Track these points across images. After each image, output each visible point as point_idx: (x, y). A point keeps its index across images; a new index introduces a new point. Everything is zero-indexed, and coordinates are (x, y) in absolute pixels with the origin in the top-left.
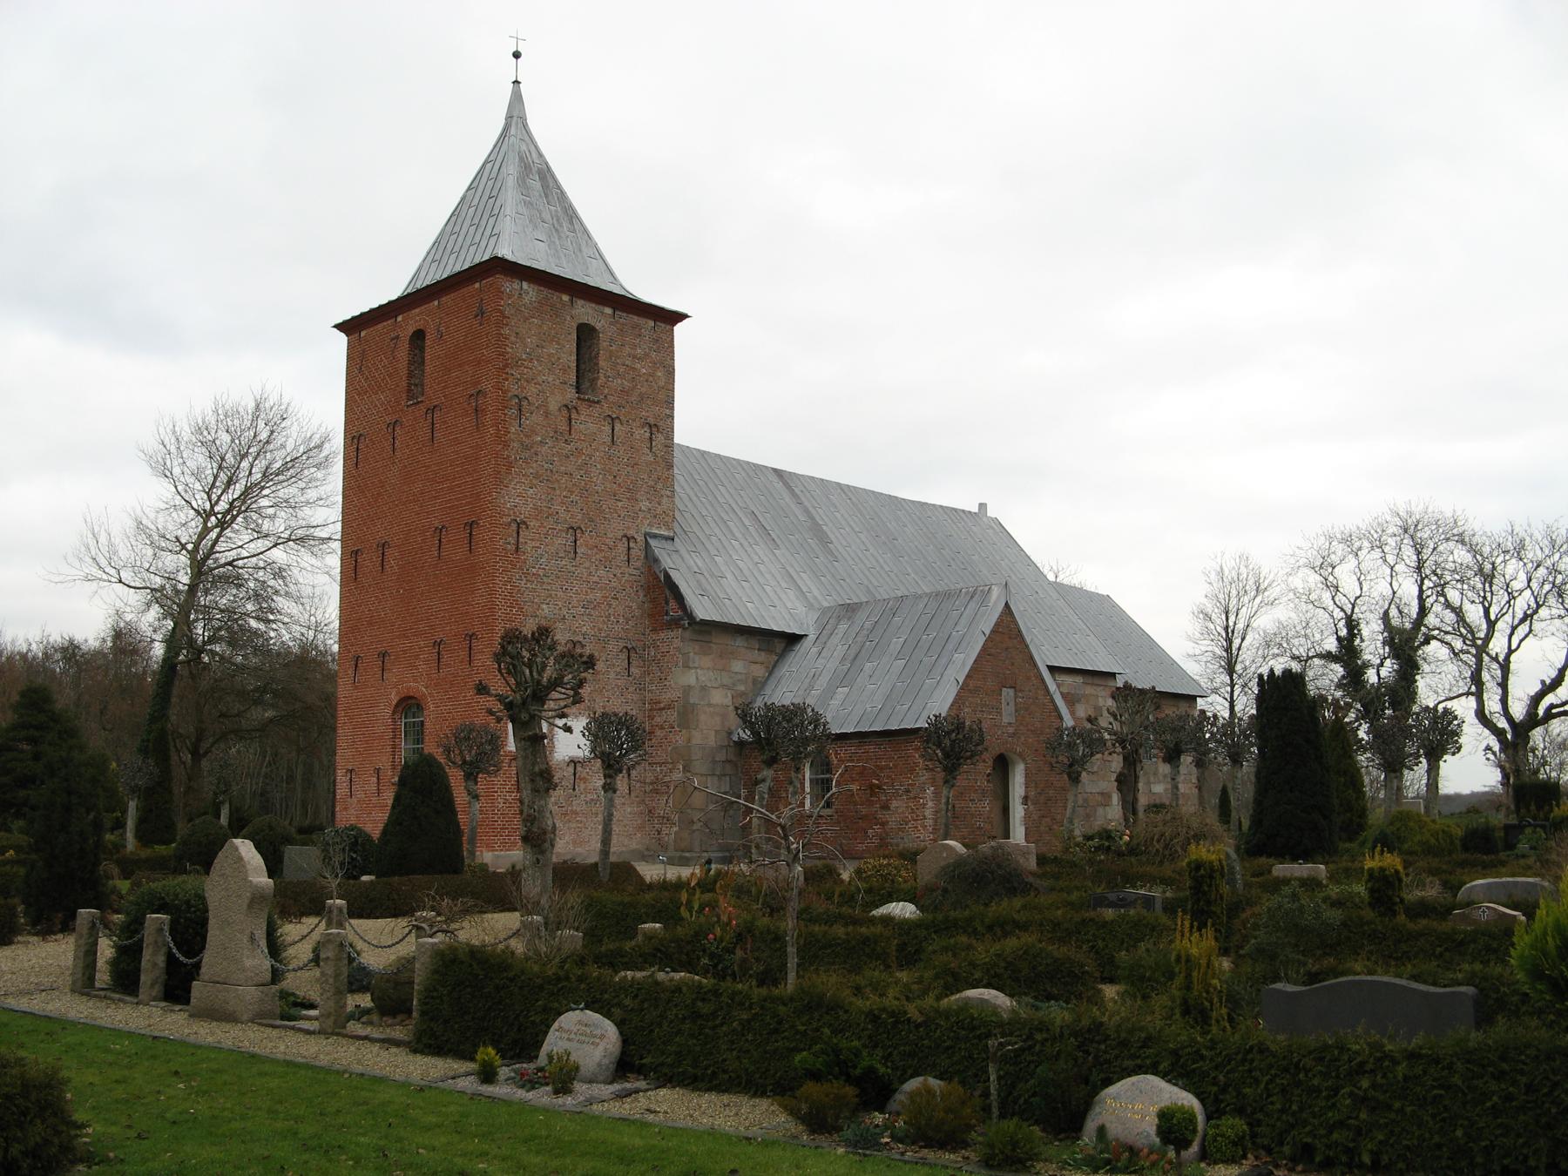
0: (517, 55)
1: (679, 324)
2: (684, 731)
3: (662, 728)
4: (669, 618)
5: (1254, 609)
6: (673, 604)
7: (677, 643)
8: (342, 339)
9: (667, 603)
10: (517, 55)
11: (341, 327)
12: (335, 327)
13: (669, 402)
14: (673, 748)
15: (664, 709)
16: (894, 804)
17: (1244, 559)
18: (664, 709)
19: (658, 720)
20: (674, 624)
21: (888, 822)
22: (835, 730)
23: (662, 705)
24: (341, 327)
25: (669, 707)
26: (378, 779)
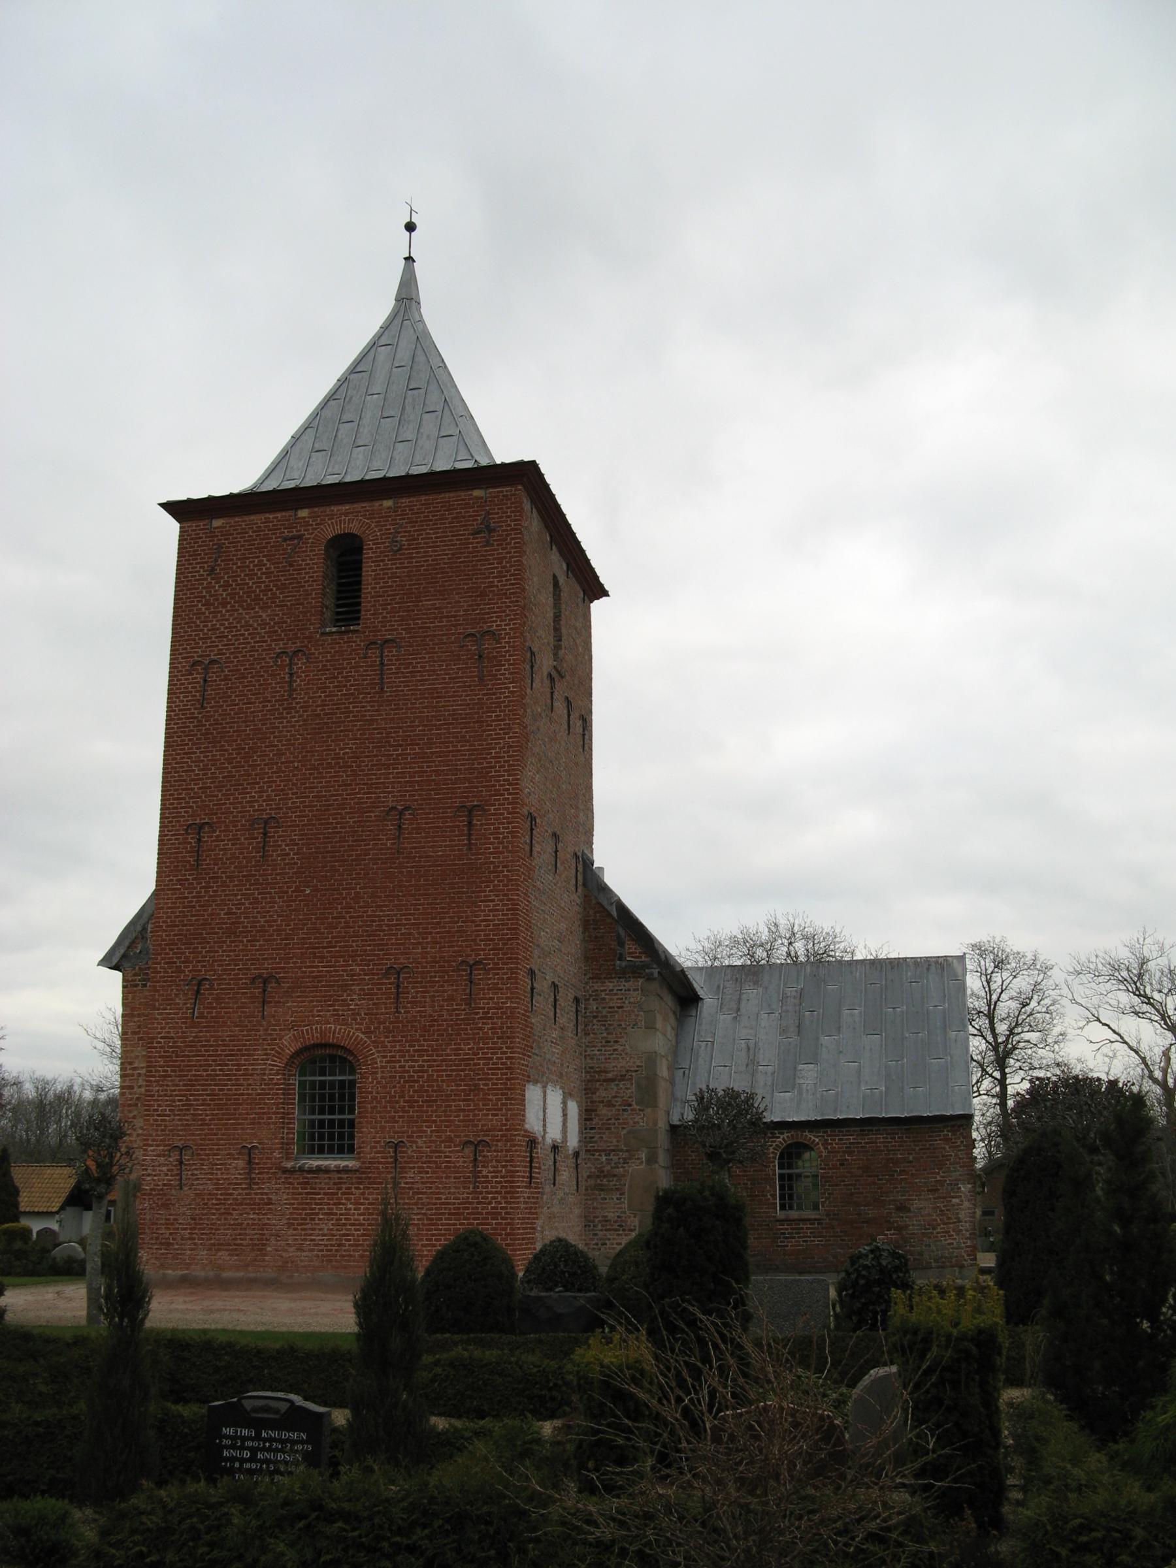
0: (410, 227)
1: (596, 602)
2: (649, 1110)
3: (609, 1104)
4: (624, 964)
5: (1153, 1011)
6: (630, 946)
7: (635, 996)
8: (172, 527)
9: (621, 944)
10: (410, 227)
11: (172, 508)
12: (162, 505)
13: (177, 599)
14: (629, 1132)
15: (613, 1080)
16: (916, 1204)
17: (1003, 940)
18: (613, 1080)
19: (602, 1093)
20: (635, 971)
21: (906, 1227)
22: (769, 1117)
23: (610, 1075)
24: (172, 508)
25: (622, 1078)
26: (250, 1162)
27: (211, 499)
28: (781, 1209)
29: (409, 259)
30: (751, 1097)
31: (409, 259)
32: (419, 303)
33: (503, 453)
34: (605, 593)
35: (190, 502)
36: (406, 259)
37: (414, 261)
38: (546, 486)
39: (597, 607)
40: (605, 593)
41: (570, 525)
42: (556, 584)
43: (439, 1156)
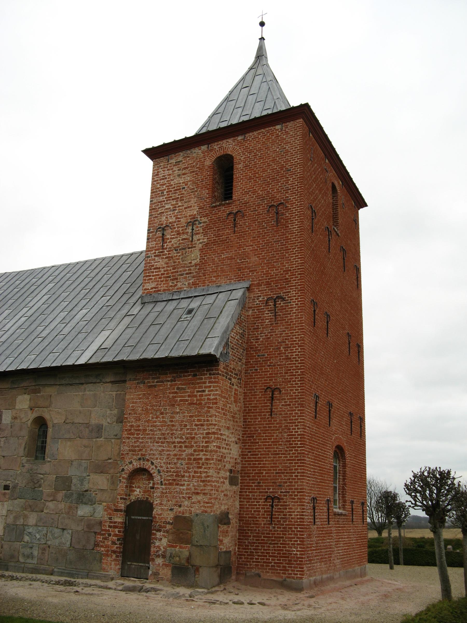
0: (262, 24)
8: (148, 163)
10: (262, 24)
27: (165, 145)
28: (336, 487)
29: (262, 39)
30: (449, 472)
31: (262, 39)
32: (267, 58)
33: (294, 102)
34: (366, 205)
35: (154, 148)
36: (260, 39)
37: (264, 39)
38: (337, 156)
39: (362, 212)
40: (366, 205)
41: (334, 149)
42: (334, 187)
43: (280, 514)
